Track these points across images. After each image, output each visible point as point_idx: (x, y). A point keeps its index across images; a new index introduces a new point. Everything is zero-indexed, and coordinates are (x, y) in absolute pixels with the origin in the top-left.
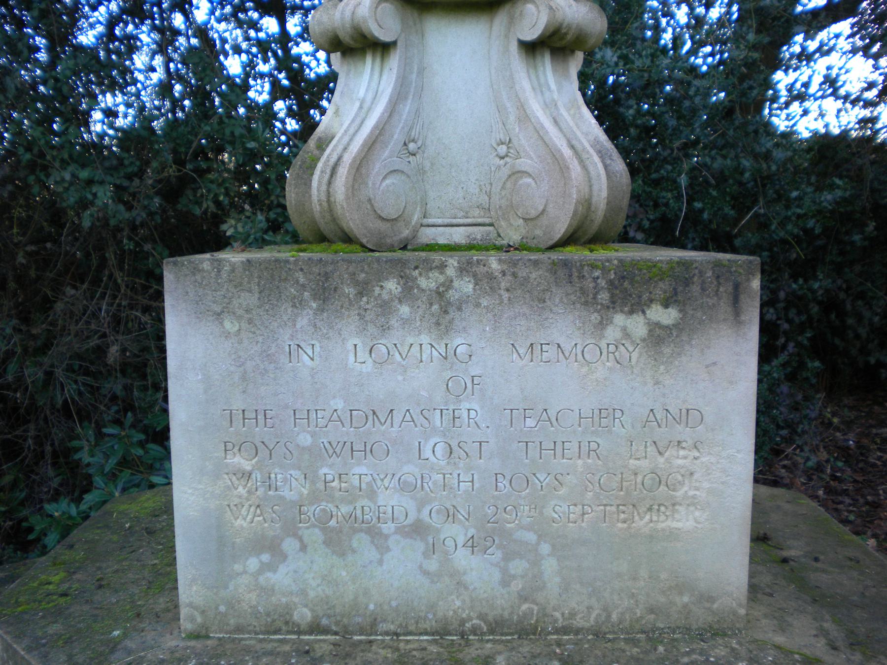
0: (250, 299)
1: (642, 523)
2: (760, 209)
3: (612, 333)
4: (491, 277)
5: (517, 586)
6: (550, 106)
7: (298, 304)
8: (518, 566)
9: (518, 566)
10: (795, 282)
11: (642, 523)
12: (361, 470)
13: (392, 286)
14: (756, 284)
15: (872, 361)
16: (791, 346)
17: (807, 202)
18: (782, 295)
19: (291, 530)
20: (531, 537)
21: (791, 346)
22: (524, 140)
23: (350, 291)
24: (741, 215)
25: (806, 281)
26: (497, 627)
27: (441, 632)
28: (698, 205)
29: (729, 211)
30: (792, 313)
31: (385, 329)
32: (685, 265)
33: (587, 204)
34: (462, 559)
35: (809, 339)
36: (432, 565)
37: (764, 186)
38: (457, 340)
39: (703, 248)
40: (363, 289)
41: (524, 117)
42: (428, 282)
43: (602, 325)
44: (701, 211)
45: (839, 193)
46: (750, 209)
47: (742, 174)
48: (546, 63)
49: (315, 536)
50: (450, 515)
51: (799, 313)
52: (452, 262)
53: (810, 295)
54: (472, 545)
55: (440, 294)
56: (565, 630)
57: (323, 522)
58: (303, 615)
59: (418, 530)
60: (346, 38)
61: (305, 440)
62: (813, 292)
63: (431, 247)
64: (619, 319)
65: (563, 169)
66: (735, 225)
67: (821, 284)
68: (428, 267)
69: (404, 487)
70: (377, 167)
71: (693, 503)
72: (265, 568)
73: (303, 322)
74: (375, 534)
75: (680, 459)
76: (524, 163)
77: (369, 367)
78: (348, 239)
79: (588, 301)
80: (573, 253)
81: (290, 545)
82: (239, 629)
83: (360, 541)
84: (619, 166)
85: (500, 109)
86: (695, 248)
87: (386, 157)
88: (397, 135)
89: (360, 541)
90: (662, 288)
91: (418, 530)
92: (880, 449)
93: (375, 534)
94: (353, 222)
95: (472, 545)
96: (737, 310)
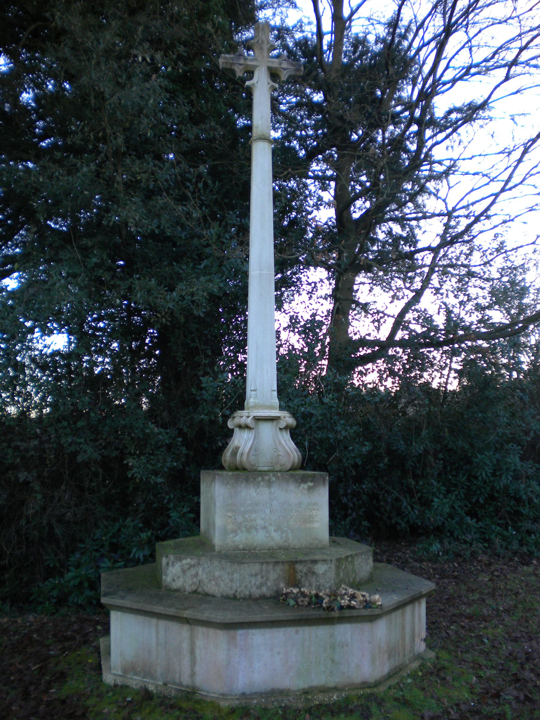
0: (233, 481)
1: (308, 525)
2: (337, 454)
3: (301, 488)
4: (278, 477)
5: (284, 539)
6: (285, 441)
7: (242, 482)
8: (284, 535)
9: (284, 535)
10: (355, 485)
11: (308, 525)
12: (253, 516)
13: (260, 479)
14: (328, 478)
15: (393, 522)
16: (354, 514)
17: (356, 451)
18: (349, 491)
19: (239, 528)
20: (286, 529)
21: (354, 514)
22: (280, 449)
23: (252, 480)
24: (330, 456)
25: (359, 485)
26: (280, 548)
27: (269, 550)
28: (312, 453)
29: (325, 456)
30: (355, 500)
31: (258, 487)
32: (314, 474)
33: (294, 462)
34: (273, 534)
35: (364, 512)
36: (267, 535)
37: (338, 444)
38: (272, 490)
39: (314, 470)
40: (254, 479)
41: (280, 443)
42: (267, 478)
43: (299, 486)
44: (314, 455)
45: (367, 448)
46: (333, 454)
47: (329, 440)
48: (284, 432)
49: (244, 529)
50: (271, 524)
51: (358, 500)
52: (271, 474)
53: (361, 491)
54: (275, 531)
55: (269, 480)
56: (293, 549)
57: (245, 527)
58: (241, 547)
59: (264, 528)
60: (243, 426)
61: (243, 509)
62: (363, 490)
63: (261, 471)
64: (302, 485)
65: (289, 455)
66: (328, 461)
67: (366, 486)
68: (267, 475)
69: (262, 519)
70: (251, 454)
71: (317, 521)
72: (235, 536)
73: (243, 486)
74: (256, 529)
75: (315, 513)
76: (281, 453)
77: (255, 495)
78: (244, 469)
79: (296, 481)
80: (291, 472)
81: (239, 531)
82: (228, 550)
83: (253, 530)
84: (299, 454)
85: (275, 442)
86: (310, 470)
87: (252, 451)
88: (254, 448)
89: (253, 530)
90: (310, 479)
91: (264, 528)
92: (396, 561)
93: (256, 529)
94: (247, 466)
95: (275, 531)
96: (324, 480)
